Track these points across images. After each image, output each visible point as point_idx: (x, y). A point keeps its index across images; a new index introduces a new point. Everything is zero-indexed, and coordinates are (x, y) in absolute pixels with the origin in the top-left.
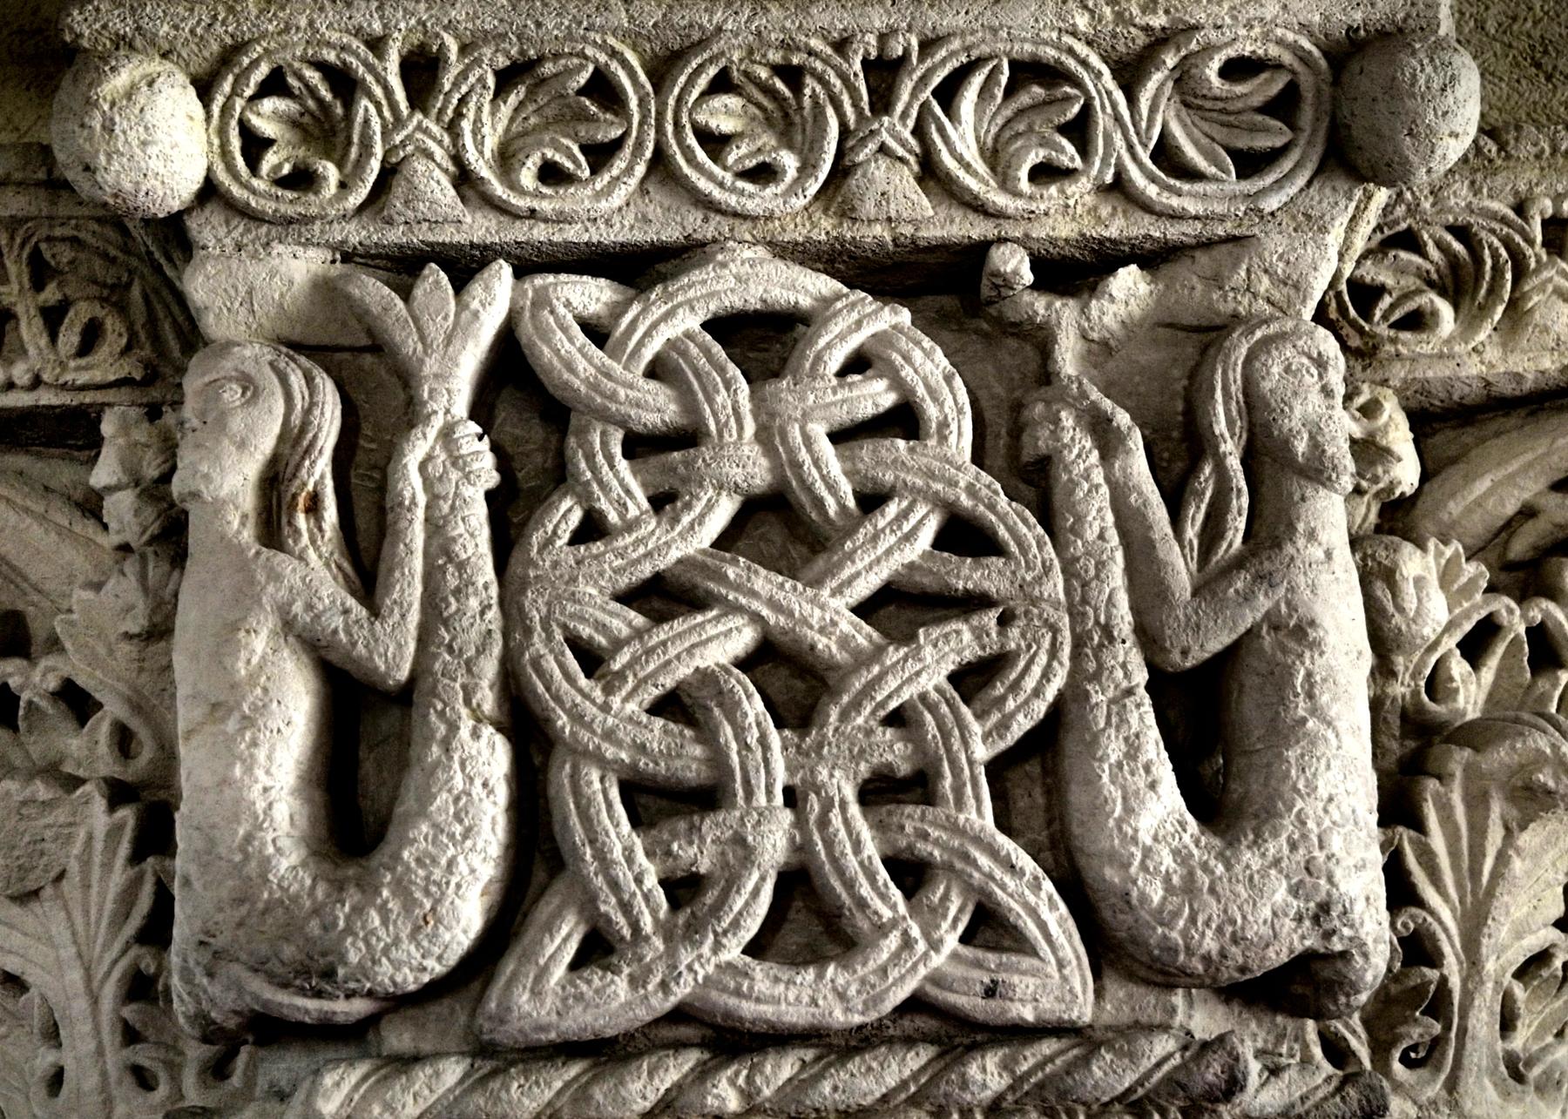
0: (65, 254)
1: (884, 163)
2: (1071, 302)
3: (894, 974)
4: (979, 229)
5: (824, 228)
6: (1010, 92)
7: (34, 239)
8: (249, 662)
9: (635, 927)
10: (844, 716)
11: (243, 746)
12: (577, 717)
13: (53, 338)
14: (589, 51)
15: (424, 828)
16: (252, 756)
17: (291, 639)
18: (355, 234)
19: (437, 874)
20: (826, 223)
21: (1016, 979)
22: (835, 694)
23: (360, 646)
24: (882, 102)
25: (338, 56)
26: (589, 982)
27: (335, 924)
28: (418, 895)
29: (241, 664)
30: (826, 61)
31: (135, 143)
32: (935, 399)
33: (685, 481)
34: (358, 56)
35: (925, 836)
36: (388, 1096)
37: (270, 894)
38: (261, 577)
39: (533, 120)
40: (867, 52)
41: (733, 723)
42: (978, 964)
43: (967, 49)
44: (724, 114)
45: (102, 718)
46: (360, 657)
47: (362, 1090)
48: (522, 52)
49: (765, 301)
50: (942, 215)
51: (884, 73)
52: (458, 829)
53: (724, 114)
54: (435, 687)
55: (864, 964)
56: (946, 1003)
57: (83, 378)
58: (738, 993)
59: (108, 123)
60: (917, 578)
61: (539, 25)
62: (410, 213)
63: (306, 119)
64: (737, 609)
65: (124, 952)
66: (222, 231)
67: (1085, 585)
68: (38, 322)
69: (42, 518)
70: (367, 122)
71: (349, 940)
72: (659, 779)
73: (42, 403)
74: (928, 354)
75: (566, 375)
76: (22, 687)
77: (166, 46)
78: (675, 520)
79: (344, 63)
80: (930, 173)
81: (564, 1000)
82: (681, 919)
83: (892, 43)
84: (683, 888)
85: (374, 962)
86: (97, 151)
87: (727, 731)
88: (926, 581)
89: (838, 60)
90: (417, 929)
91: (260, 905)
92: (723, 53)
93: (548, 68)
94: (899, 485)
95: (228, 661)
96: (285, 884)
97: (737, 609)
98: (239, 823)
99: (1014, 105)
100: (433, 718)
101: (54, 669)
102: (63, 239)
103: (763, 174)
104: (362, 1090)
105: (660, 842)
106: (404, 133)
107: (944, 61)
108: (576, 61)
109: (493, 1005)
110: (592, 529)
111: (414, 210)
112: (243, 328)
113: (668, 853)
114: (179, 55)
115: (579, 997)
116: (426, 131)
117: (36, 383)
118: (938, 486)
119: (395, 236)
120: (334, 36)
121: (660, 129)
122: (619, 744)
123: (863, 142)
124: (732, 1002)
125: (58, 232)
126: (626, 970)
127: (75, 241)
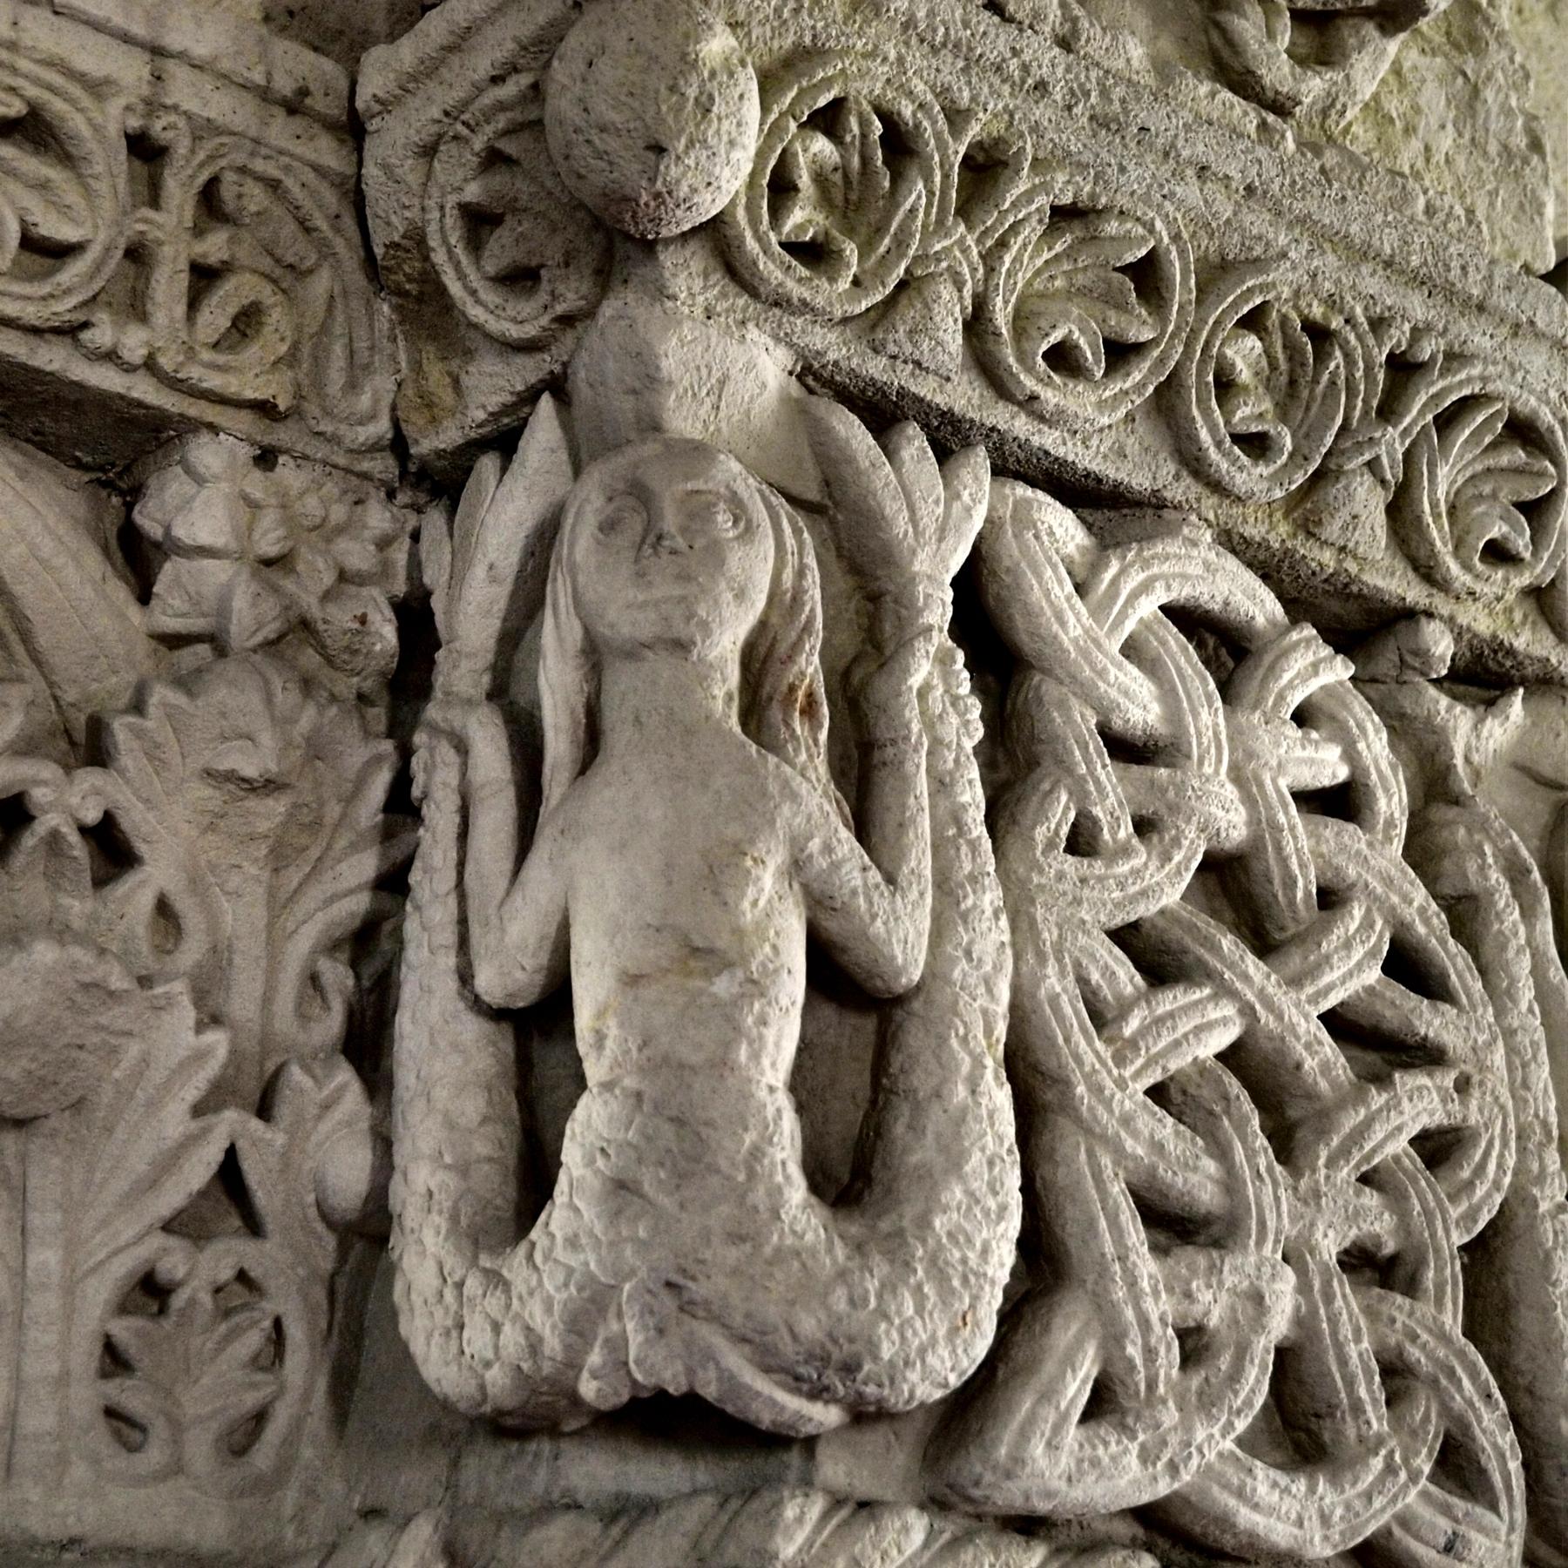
0: (256, 198)
1: (1368, 479)
2: (1469, 713)
3: (1378, 1502)
4: (1414, 593)
5: (1278, 534)
6: (1494, 446)
7: (223, 163)
8: (755, 903)
9: (1151, 1385)
10: (1331, 1163)
11: (750, 1020)
12: (1097, 1090)
13: (193, 304)
14: (1159, 225)
15: (958, 1193)
16: (761, 1037)
17: (796, 886)
18: (833, 347)
19: (973, 1257)
20: (1284, 529)
21: (1473, 1535)
22: (1323, 1133)
23: (879, 923)
24: (1388, 411)
25: (914, 114)
26: (1106, 1444)
27: (866, 1300)
28: (956, 1283)
29: (746, 905)
30: (1359, 338)
31: (725, 138)
32: (1386, 790)
33: (1174, 809)
34: (934, 123)
35: (1414, 1337)
36: (857, 1549)
37: (781, 1237)
38: (773, 787)
39: (1058, 283)
40: (1399, 343)
41: (1244, 1142)
42: (1446, 1510)
43: (1484, 379)
44: (1245, 354)
45: (142, 884)
46: (877, 936)
47: (826, 1533)
48: (1093, 196)
49: (1226, 603)
50: (1386, 563)
51: (1403, 370)
52: (992, 1204)
53: (1245, 354)
54: (956, 1003)
55: (1354, 1484)
56: (1407, 1551)
57: (214, 381)
58: (1240, 1494)
59: (704, 99)
60: (1379, 1007)
61: (1122, 169)
62: (908, 348)
63: (837, 178)
64: (1233, 994)
65: (139, 1239)
66: (698, 284)
67: (1525, 1066)
68: (183, 280)
69: (76, 558)
70: (913, 211)
71: (883, 1326)
72: (1174, 1193)
73: (135, 394)
74: (1377, 731)
75: (1055, 627)
76: (52, 806)
77: (741, 17)
78: (1166, 858)
79: (917, 126)
80: (1400, 511)
81: (1080, 1461)
82: (1195, 1381)
83: (1425, 343)
84: (1194, 1343)
85: (906, 1363)
86: (681, 131)
87: (1238, 1146)
88: (1388, 1013)
89: (1371, 341)
90: (954, 1332)
91: (768, 1250)
92: (1274, 285)
93: (1112, 227)
94: (1361, 885)
95: (730, 894)
96: (798, 1228)
97: (1233, 994)
98: (746, 1129)
99: (1491, 462)
100: (954, 1043)
101: (97, 792)
102: (259, 178)
103: (1256, 445)
104: (826, 1533)
105: (1177, 1277)
106: (946, 243)
107: (1461, 384)
108: (1141, 230)
109: (1003, 1451)
110: (1082, 841)
111: (915, 345)
112: (699, 426)
113: (1188, 1295)
114: (749, 34)
115: (1095, 1463)
116: (965, 250)
117: (150, 365)
118: (1395, 899)
119: (876, 368)
120: (919, 87)
121: (1189, 345)
122: (1135, 1134)
123: (1359, 447)
124: (1232, 1502)
125: (259, 165)
126: (1141, 1437)
127: (273, 185)
